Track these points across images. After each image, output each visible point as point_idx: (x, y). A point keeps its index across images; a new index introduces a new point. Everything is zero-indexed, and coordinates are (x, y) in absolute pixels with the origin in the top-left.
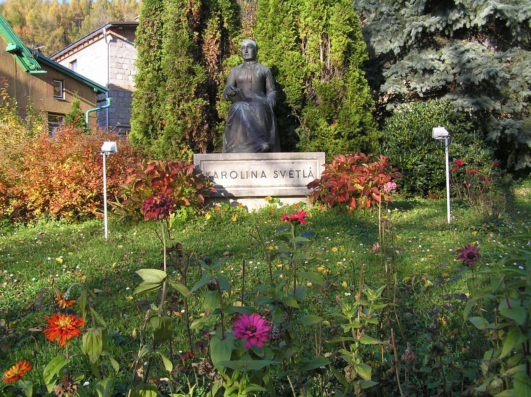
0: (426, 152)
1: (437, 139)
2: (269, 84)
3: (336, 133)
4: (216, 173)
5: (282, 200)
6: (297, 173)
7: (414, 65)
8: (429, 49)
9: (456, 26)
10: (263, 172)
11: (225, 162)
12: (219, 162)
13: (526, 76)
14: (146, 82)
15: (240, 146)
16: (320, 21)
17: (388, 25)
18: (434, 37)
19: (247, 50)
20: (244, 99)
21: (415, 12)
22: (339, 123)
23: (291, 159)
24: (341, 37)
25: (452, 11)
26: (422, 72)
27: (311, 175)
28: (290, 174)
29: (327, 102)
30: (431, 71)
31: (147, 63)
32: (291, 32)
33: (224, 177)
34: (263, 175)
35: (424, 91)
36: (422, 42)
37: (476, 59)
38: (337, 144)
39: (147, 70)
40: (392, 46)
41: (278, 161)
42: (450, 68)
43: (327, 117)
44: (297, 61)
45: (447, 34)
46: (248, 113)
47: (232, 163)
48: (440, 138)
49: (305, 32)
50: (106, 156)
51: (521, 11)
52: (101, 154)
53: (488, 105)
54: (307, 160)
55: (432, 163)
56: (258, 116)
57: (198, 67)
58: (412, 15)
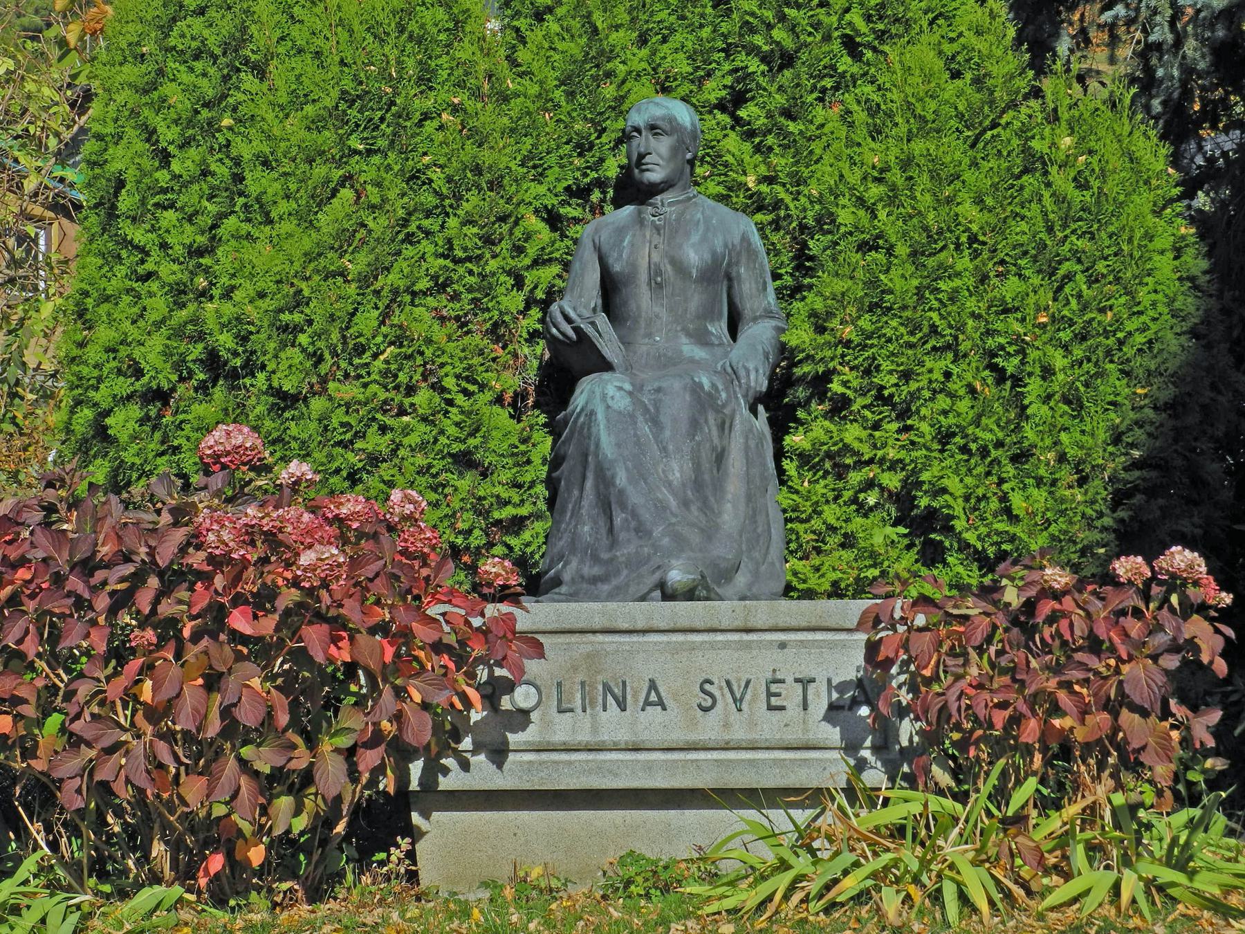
10: (653, 686)
28: (770, 694)
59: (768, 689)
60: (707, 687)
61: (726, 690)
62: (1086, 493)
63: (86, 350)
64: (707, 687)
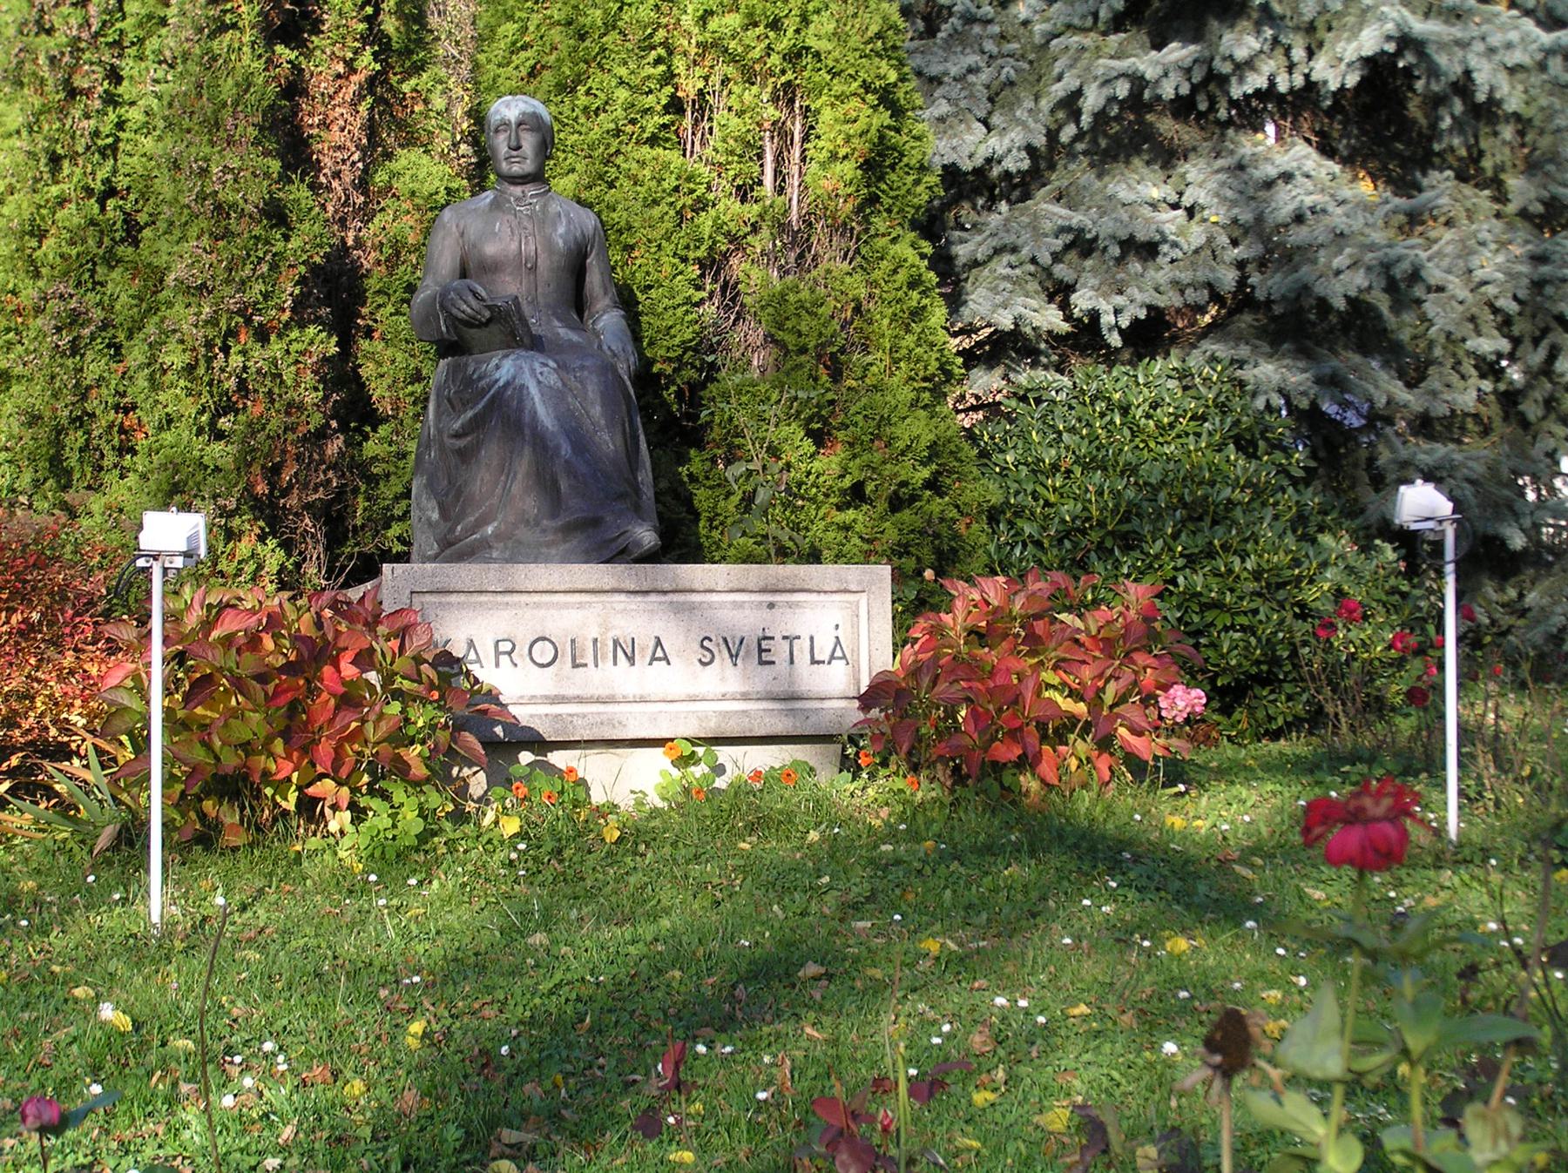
0: (1181, 562)
1: (1414, 527)
2: (594, 279)
3: (847, 482)
4: (471, 644)
5: (724, 754)
6: (786, 644)
7: (1089, 224)
8: (1137, 162)
9: (1241, 80)
10: (659, 643)
11: (508, 598)
12: (483, 598)
13: (1486, 283)
14: (49, 242)
15: (524, 533)
16: (772, 34)
17: (972, 59)
18: (1149, 117)
19: (518, 138)
20: (526, 340)
21: (1083, 17)
22: (851, 445)
23: (763, 591)
24: (855, 103)
25: (1232, 26)
26: (1115, 251)
27: (838, 653)
28: (761, 651)
29: (803, 358)
30: (1149, 250)
31: (55, 160)
32: (652, 71)
33: (504, 659)
34: (659, 654)
35: (1125, 323)
36: (1106, 135)
37: (1324, 211)
38: (846, 528)
39: (54, 190)
40: (996, 144)
41: (714, 597)
42: (1223, 240)
43: (810, 420)
44: (676, 189)
45: (1203, 106)
46: (556, 397)
47: (537, 605)
48: (1430, 525)
49: (699, 72)
50: (165, 570)
51: (1479, 47)
52: (141, 563)
53: (1371, 389)
54: (822, 597)
55: (1206, 607)
56: (597, 411)
57: (299, 193)
58: (1069, 26)
59: (760, 645)
60: (706, 643)
61: (723, 647)
62: (115, 337)
63: (1368, 513)
64: (706, 643)
